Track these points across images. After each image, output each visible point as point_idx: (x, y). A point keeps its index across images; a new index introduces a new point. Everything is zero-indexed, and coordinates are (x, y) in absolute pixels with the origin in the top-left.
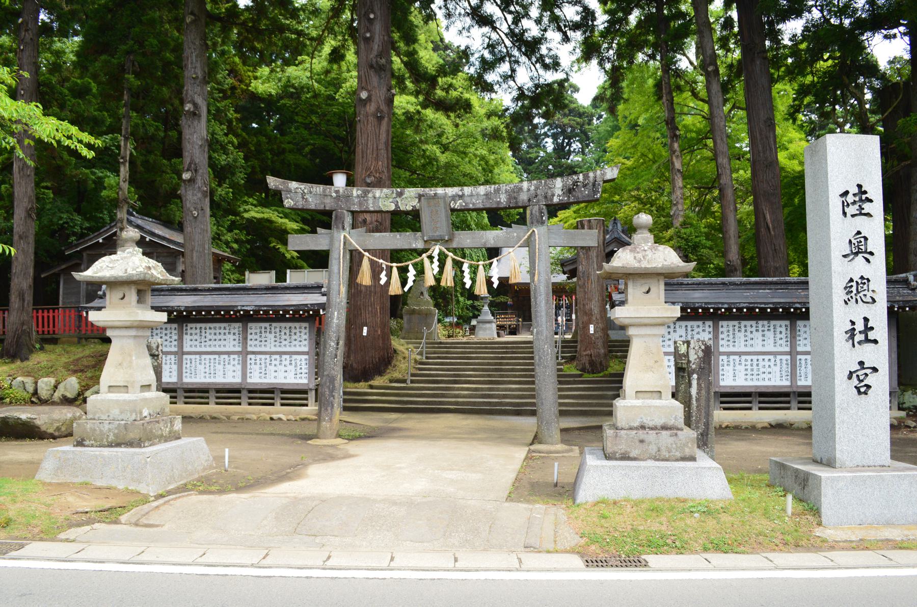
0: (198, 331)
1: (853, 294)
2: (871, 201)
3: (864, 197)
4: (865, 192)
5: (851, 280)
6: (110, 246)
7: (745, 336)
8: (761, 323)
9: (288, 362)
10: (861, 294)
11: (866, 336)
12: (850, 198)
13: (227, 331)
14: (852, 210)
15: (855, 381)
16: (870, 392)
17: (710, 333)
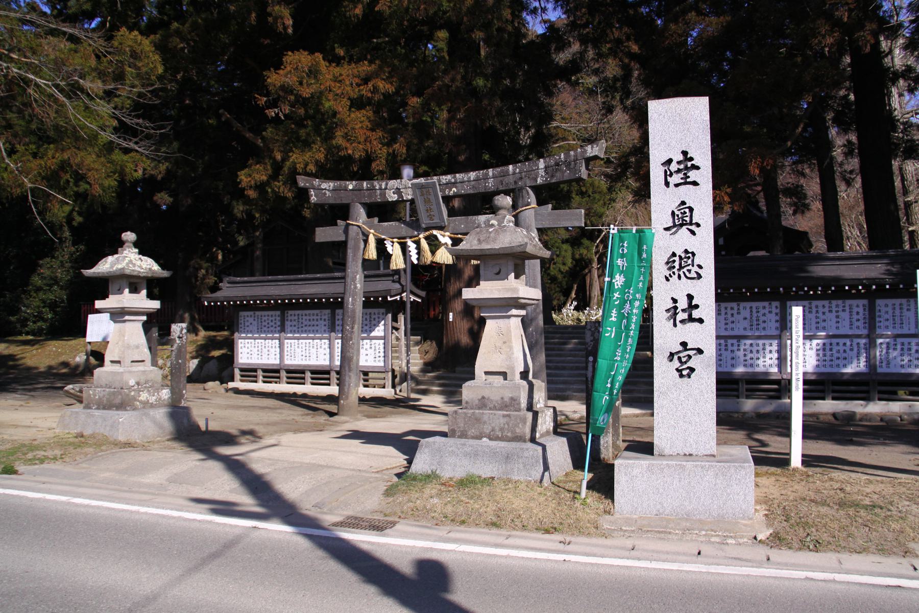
0: (296, 318)
1: (675, 270)
2: (698, 168)
3: (689, 164)
4: (691, 159)
5: (674, 255)
6: (115, 246)
7: (817, 317)
8: (834, 302)
9: (368, 346)
10: (685, 270)
11: (690, 315)
12: (674, 167)
13: (319, 317)
14: (676, 179)
15: (676, 363)
16: (693, 375)
17: (777, 314)
